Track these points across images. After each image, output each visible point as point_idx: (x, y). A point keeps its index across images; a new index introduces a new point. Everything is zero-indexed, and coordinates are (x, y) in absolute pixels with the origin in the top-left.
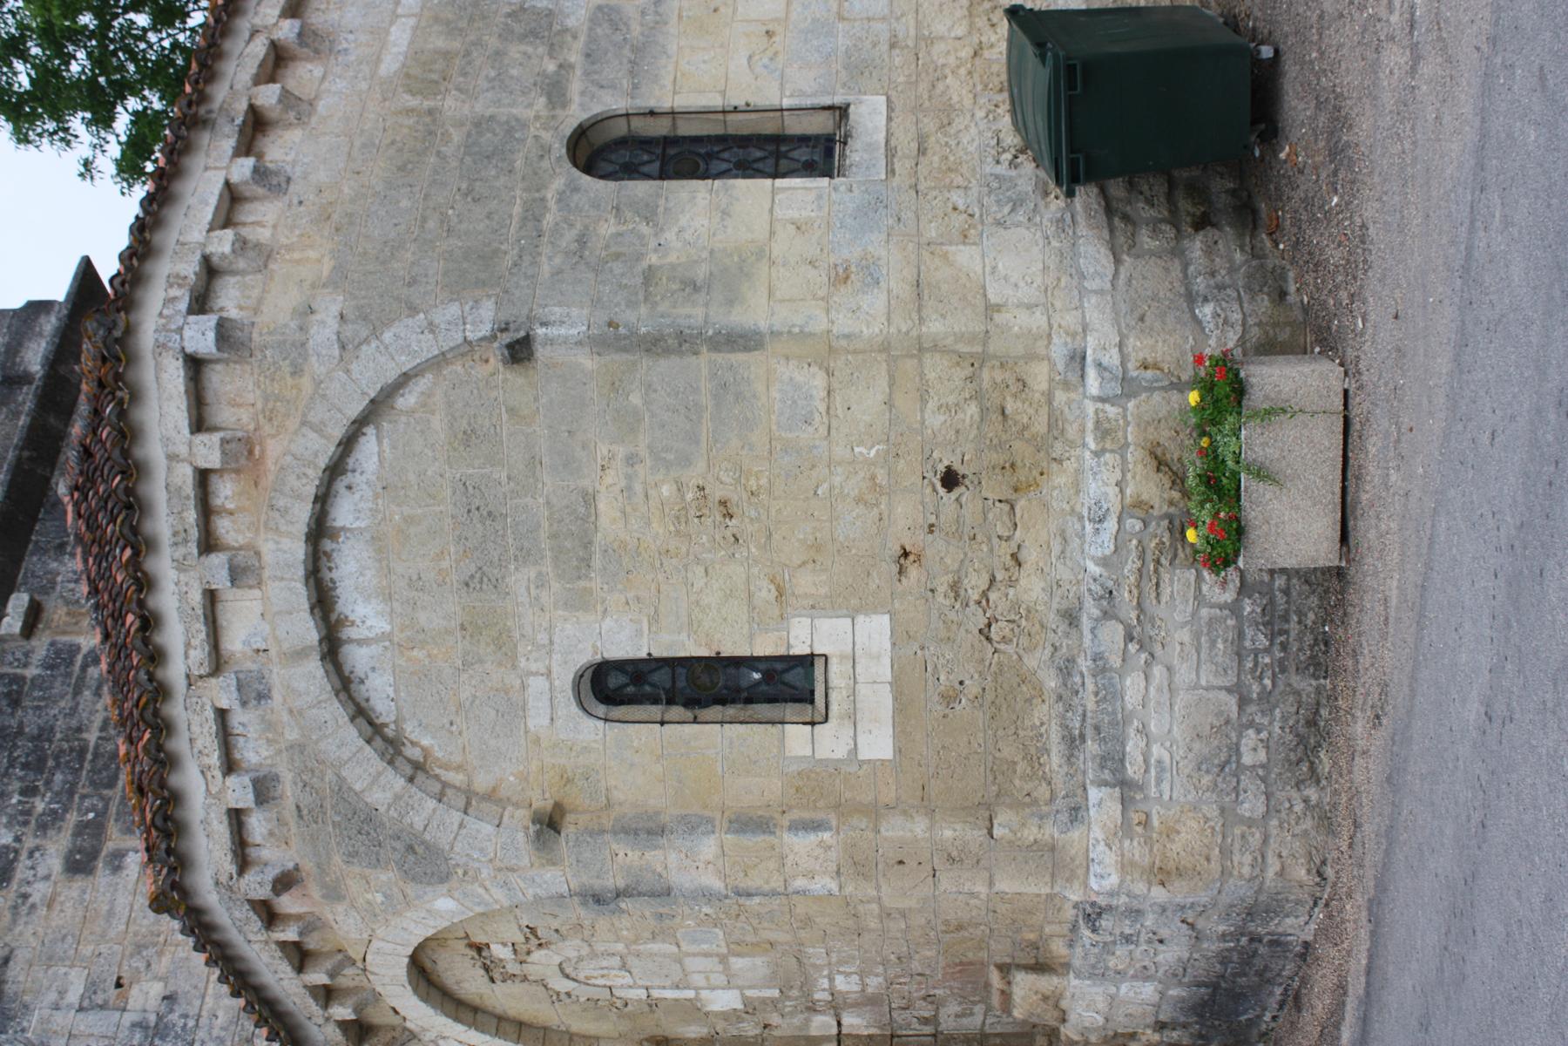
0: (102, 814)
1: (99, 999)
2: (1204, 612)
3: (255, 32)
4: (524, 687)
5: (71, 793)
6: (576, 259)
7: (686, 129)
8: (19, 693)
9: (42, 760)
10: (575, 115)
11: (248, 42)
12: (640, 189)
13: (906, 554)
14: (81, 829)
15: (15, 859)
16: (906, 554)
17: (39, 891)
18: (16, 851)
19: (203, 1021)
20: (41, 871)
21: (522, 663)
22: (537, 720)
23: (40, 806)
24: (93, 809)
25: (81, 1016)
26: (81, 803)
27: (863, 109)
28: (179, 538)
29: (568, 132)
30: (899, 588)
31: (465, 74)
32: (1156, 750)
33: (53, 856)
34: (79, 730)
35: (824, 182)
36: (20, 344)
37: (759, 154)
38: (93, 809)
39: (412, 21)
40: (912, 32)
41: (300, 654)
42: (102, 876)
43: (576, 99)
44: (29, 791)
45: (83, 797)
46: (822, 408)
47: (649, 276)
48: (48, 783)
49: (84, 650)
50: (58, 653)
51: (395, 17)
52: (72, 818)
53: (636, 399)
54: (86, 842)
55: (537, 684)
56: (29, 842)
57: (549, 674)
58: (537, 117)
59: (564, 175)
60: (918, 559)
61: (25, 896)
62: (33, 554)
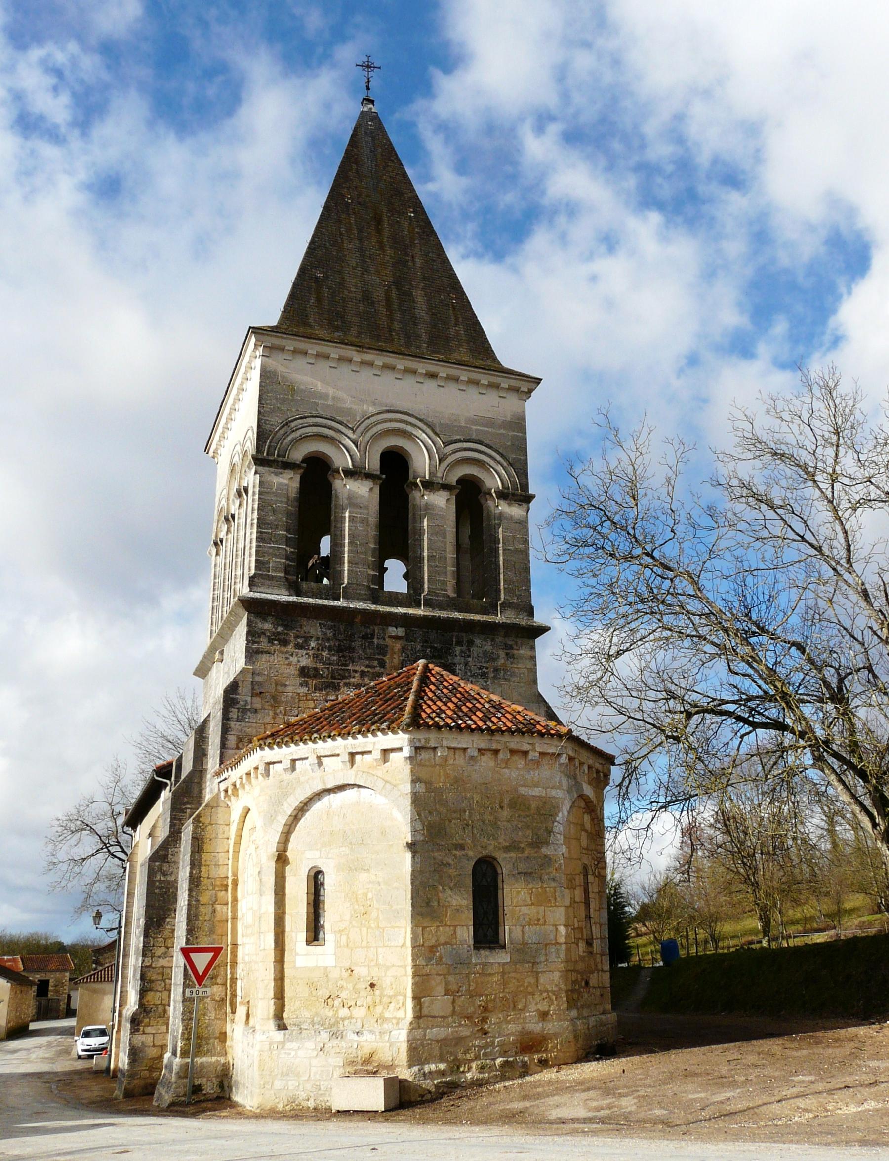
0: (322, 676)
1: (256, 687)
2: (331, 1069)
3: (533, 744)
4: (317, 850)
5: (330, 664)
6: (440, 863)
7: (500, 892)
8: (368, 638)
9: (342, 651)
10: (500, 856)
11: (528, 743)
12: (469, 881)
13: (352, 971)
14: (316, 669)
15: (305, 649)
16: (352, 971)
17: (294, 659)
18: (308, 649)
19: (248, 724)
20: (300, 659)
21: (323, 850)
22: (309, 854)
23: (325, 654)
24: (324, 672)
25: (250, 683)
26: (326, 668)
27: (504, 954)
28: (353, 746)
29: (493, 855)
30: (343, 969)
31: (519, 816)
32: (293, 1053)
33: (305, 662)
34: (353, 662)
35: (472, 942)
36: (513, 608)
37: (490, 918)
38: (324, 672)
39: (544, 795)
40: (540, 970)
41: (324, 782)
42: (298, 681)
43: (507, 856)
44: (330, 649)
45: (328, 668)
46: (392, 944)
47: (434, 887)
48: (334, 655)
49: (385, 658)
50: (383, 649)
51: (546, 788)
52: (320, 666)
53: (395, 885)
54: (312, 672)
55: (317, 854)
56: (311, 653)
57: (320, 857)
58: (499, 844)
59: (474, 855)
60: (350, 975)
61: (292, 655)
62: (423, 632)
